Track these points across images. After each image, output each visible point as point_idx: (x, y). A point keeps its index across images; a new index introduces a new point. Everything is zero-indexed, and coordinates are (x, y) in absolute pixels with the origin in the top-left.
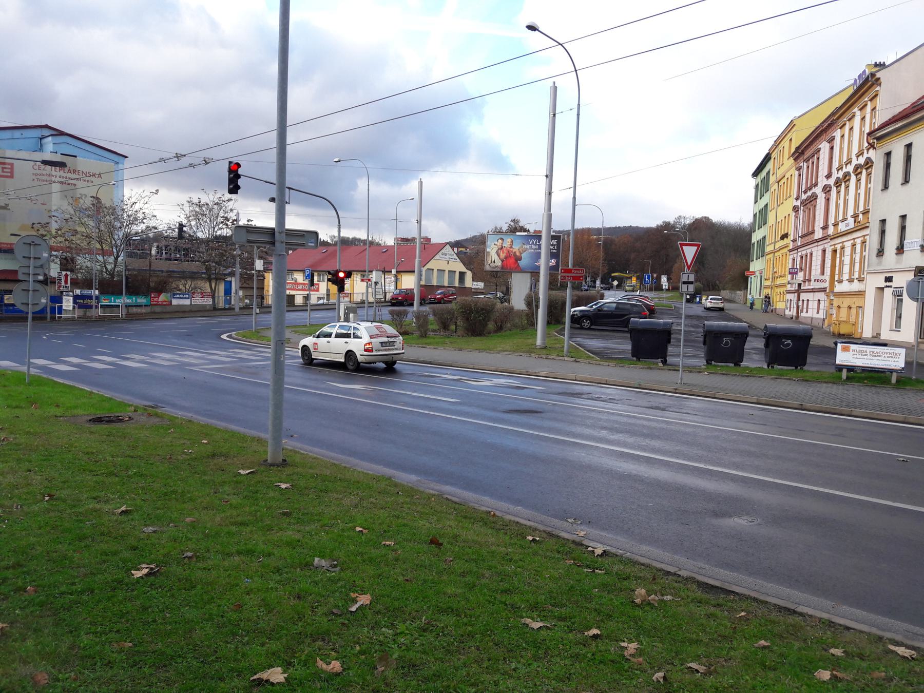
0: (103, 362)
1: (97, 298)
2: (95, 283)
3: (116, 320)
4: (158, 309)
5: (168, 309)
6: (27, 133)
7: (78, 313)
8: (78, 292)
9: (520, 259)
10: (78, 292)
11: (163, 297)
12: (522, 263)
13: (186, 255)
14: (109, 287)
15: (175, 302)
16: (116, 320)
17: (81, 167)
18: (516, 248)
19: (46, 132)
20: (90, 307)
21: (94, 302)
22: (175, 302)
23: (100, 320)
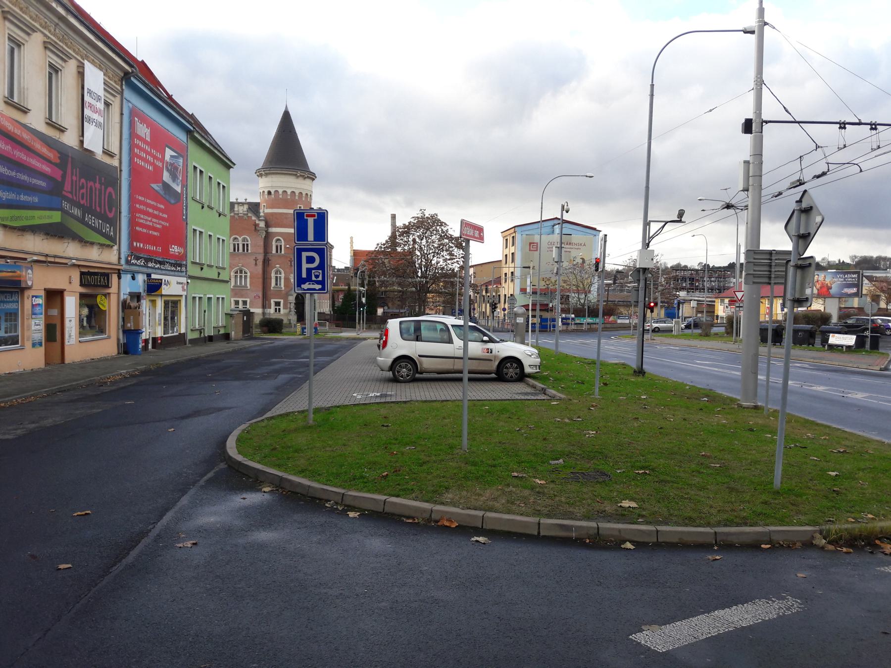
0: (13, 174)
1: (573, 319)
2: (572, 311)
3: (582, 331)
4: (608, 326)
5: (615, 326)
6: (545, 224)
7: (565, 327)
8: (564, 316)
9: (831, 288)
10: (564, 316)
11: (612, 319)
12: (832, 291)
13: (691, 284)
14: (579, 312)
15: (619, 321)
16: (582, 331)
17: (573, 241)
18: (828, 281)
19: (556, 222)
20: (568, 324)
21: (570, 321)
22: (619, 321)
23: (573, 331)
